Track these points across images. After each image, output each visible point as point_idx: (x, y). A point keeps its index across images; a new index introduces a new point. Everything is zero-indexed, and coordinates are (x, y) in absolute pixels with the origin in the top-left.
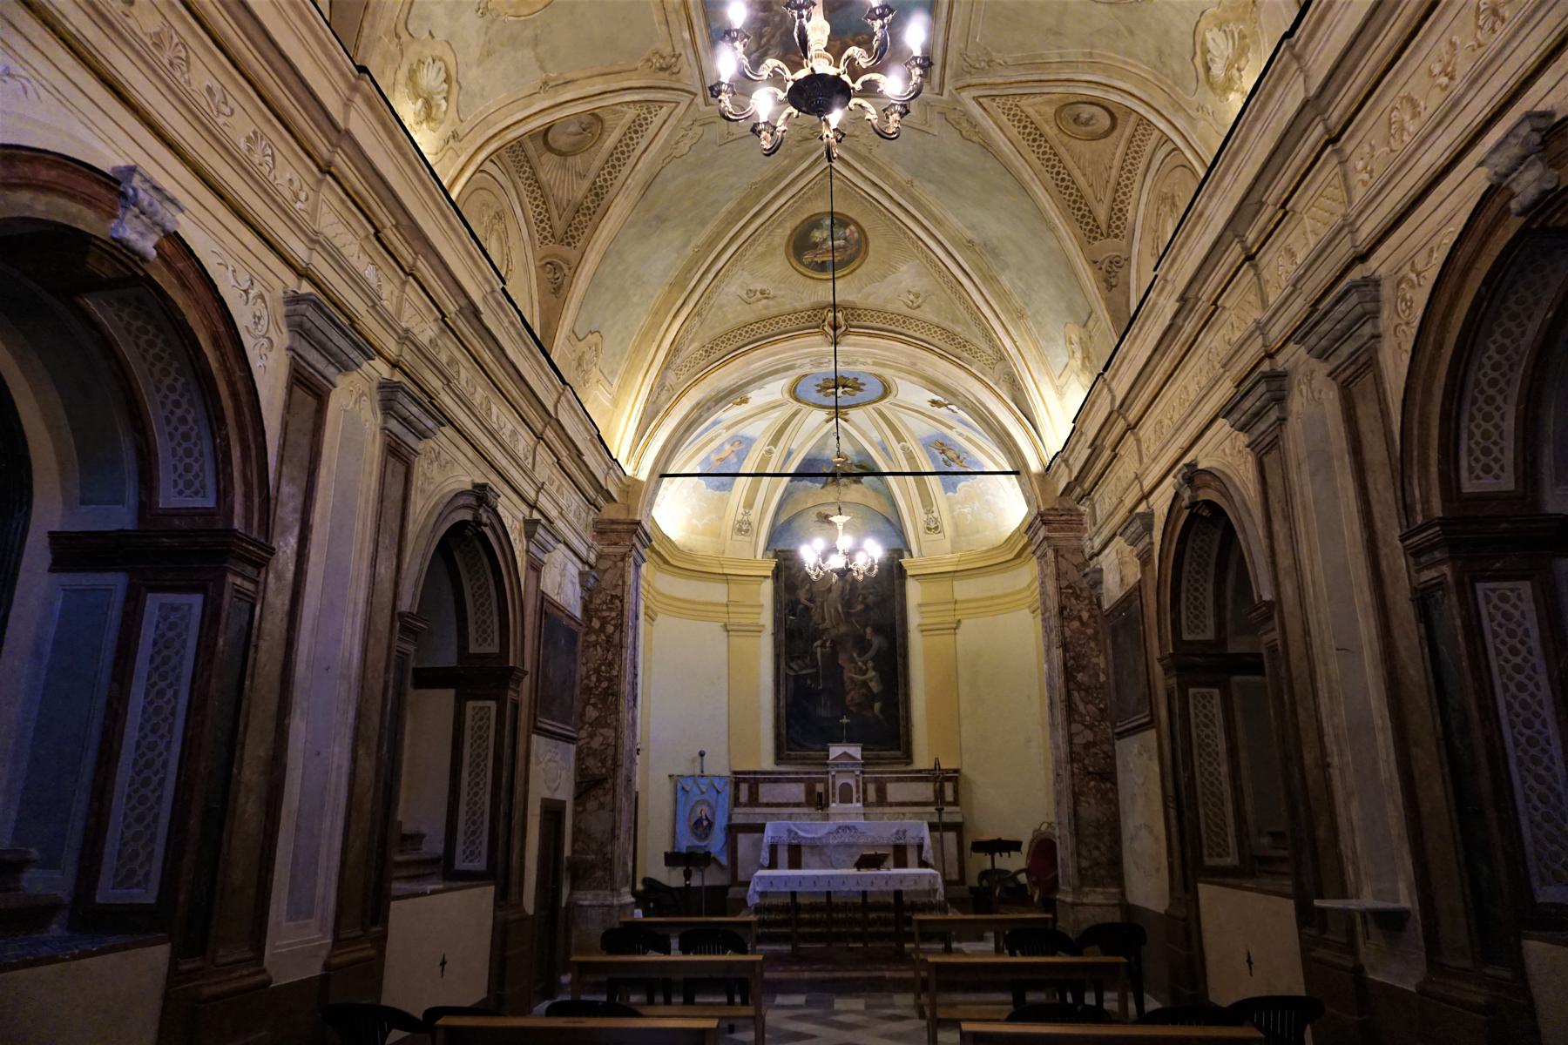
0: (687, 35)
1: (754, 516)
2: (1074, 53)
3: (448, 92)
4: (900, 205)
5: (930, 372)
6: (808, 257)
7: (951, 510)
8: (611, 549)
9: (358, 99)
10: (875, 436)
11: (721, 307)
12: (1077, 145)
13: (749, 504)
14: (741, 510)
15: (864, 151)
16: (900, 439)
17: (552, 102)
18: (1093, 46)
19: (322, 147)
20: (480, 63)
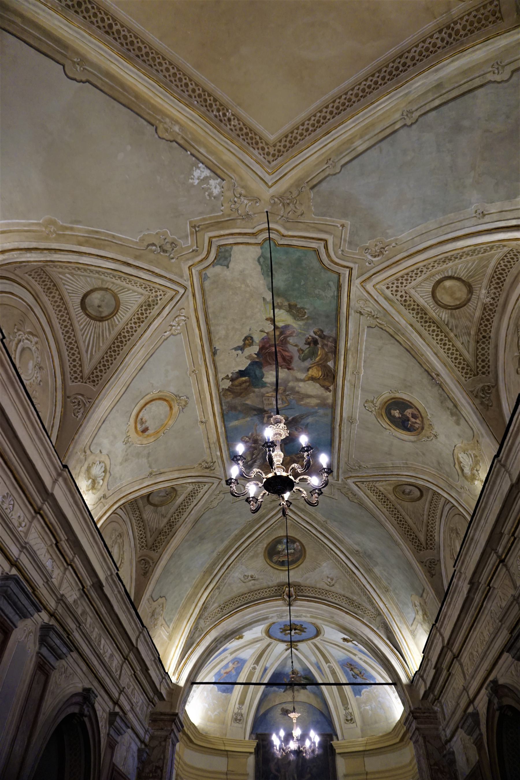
0: (219, 453)
1: (244, 710)
3: (104, 477)
4: (321, 533)
5: (341, 622)
6: (275, 558)
7: (359, 708)
8: (159, 733)
9: (60, 480)
10: (313, 659)
11: (230, 584)
13: (242, 702)
14: (237, 706)
16: (327, 661)
19: (38, 500)
20: (121, 464)
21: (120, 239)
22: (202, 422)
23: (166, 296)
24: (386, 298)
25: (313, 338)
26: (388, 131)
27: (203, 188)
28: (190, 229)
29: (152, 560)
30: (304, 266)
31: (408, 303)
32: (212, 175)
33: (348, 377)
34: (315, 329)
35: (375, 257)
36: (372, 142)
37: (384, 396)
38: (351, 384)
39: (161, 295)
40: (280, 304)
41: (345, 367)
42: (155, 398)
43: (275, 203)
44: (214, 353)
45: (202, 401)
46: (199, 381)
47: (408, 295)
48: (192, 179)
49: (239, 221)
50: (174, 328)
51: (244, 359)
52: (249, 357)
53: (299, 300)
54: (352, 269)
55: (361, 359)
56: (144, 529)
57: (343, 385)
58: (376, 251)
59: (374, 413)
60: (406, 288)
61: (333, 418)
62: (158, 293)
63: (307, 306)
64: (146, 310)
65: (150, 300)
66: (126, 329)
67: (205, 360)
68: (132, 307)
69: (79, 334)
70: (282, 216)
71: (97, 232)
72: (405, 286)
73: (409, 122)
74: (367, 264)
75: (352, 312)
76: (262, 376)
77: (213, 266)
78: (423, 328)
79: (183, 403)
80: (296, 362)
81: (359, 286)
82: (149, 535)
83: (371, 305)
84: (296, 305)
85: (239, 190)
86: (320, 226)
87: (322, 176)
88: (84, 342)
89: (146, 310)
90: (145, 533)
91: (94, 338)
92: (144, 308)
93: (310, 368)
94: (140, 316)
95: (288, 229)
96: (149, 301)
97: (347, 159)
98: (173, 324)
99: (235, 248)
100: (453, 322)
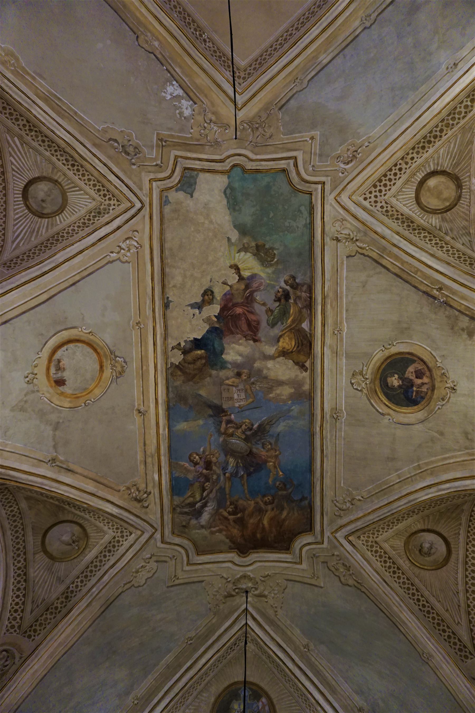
0: (156, 477)
2: (407, 470)
12: (426, 575)
15: (271, 612)
17: (54, 476)
18: (419, 459)
20: (12, 410)
21: (82, 119)
22: (140, 412)
23: (120, 207)
24: (364, 209)
25: (284, 290)
26: (350, 39)
27: (174, 105)
28: (157, 141)
29: (21, 652)
30: (273, 193)
31: (391, 213)
32: (185, 95)
33: (328, 341)
34: (286, 277)
35: (348, 163)
36: (336, 52)
37: (375, 359)
38: (332, 352)
39: (114, 205)
40: (246, 246)
41: (323, 325)
42: (82, 339)
43: (244, 128)
44: (166, 305)
45: (143, 376)
46: (143, 341)
47: (389, 206)
48: (164, 92)
49: (207, 147)
50: (122, 251)
51: (201, 321)
52: (208, 320)
53: (268, 238)
54: (324, 183)
55: (342, 307)
56: (24, 596)
57: (323, 354)
58: (348, 157)
59: (365, 391)
60: (386, 197)
61: (312, 415)
62: (112, 202)
63: (277, 246)
64: (94, 217)
65: (102, 207)
66: (66, 231)
67: (154, 311)
68: (79, 210)
69: (11, 223)
70: (251, 142)
71: (59, 99)
72: (385, 195)
73: (368, 24)
74: (340, 174)
75: (327, 240)
76: (222, 352)
77: (177, 191)
78: (412, 235)
79: (119, 369)
80: (265, 331)
81: (334, 203)
82: (29, 608)
83: (348, 225)
84: (264, 245)
85: (210, 116)
86: (289, 146)
87: (290, 94)
88: (14, 232)
89: (94, 217)
90: (23, 603)
91: (26, 232)
92: (93, 214)
93: (281, 336)
94: (86, 221)
95: (256, 154)
96: (100, 209)
97: (313, 73)
98: (123, 246)
99: (202, 176)
100: (446, 226)
